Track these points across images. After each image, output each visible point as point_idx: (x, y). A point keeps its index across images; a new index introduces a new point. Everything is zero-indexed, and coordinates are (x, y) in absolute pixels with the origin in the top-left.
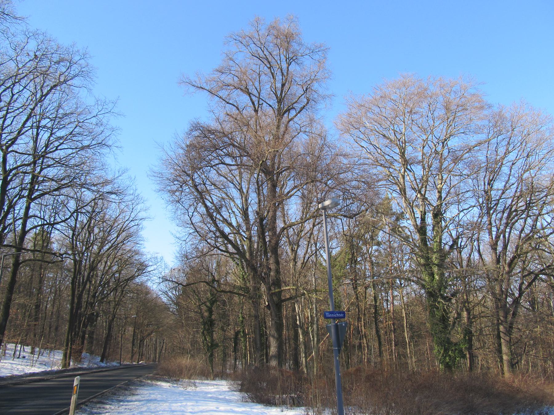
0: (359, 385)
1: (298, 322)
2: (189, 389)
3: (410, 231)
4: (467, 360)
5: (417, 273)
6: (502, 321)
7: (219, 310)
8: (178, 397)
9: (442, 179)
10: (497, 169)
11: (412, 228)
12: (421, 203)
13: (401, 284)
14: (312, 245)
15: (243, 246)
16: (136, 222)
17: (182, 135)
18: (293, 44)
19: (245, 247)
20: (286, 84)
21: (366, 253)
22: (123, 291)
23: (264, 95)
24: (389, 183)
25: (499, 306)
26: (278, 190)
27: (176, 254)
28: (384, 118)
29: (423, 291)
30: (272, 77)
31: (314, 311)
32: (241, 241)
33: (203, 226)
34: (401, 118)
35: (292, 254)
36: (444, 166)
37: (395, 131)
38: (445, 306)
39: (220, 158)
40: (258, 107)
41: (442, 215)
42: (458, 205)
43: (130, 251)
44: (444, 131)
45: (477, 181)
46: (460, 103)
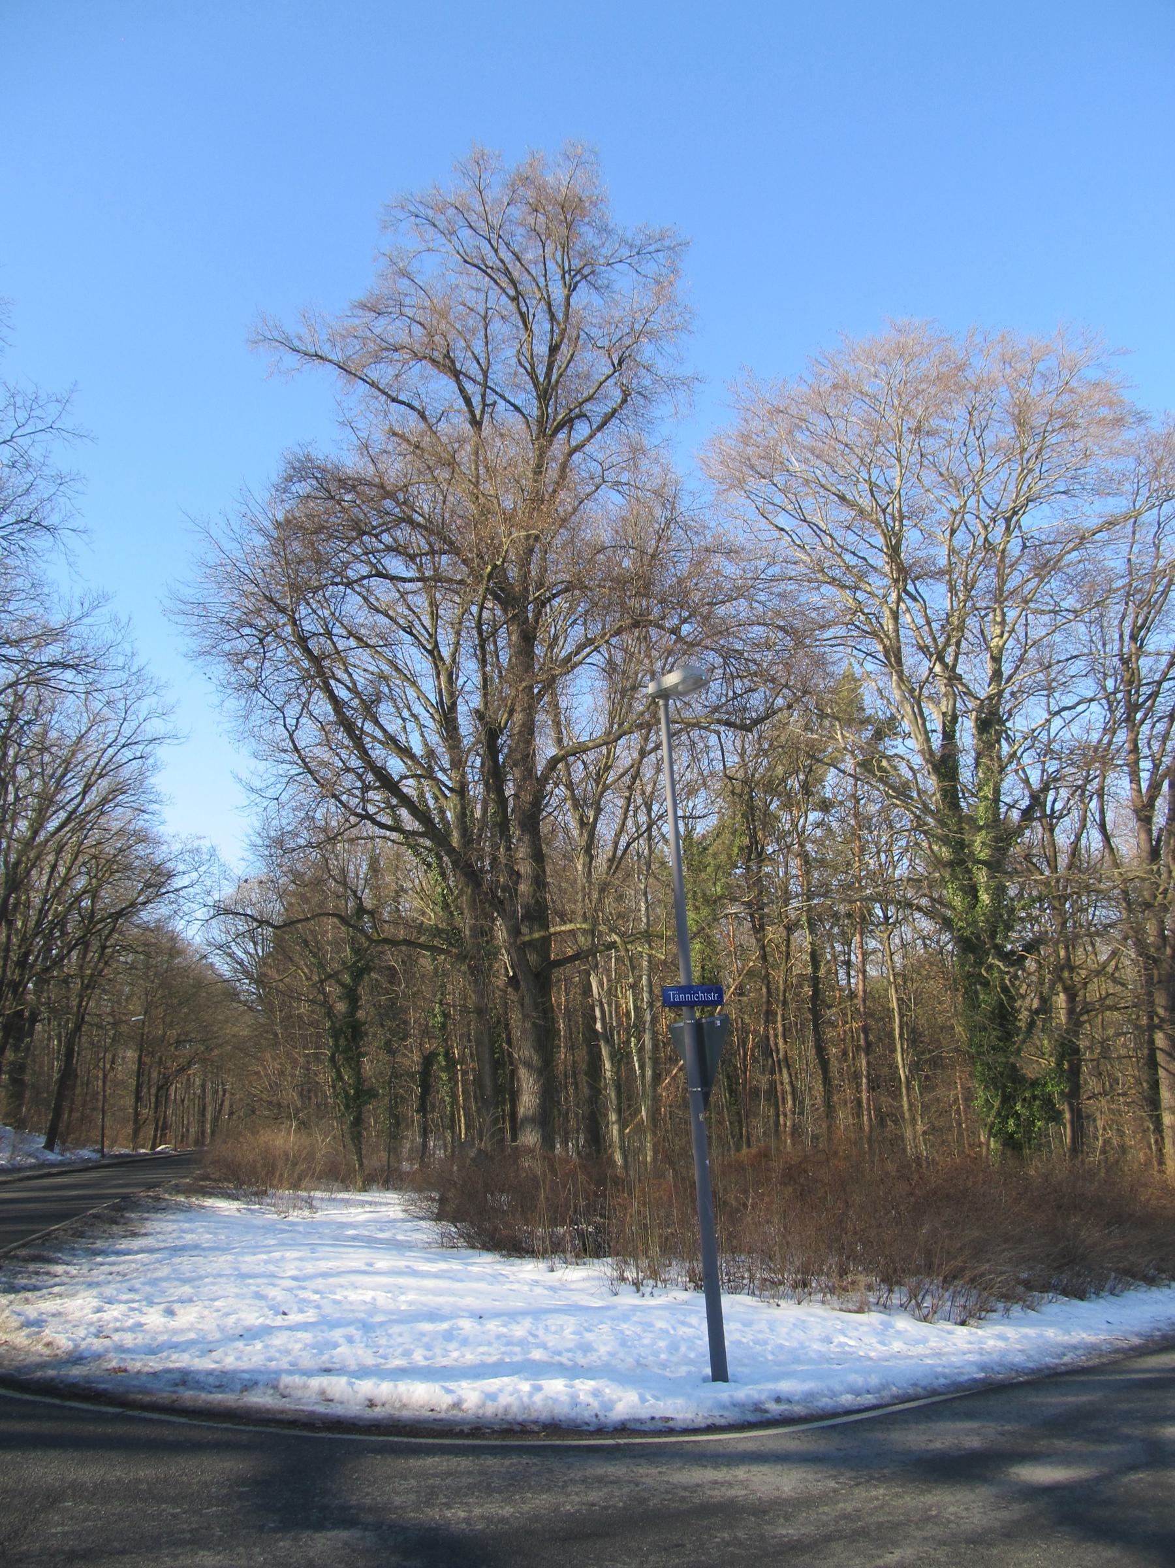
0: (763, 1194)
1: (599, 1026)
2: (295, 1216)
3: (911, 769)
4: (1065, 1128)
5: (930, 887)
6: (1162, 1020)
7: (379, 994)
8: (261, 1238)
9: (1003, 623)
10: (1156, 596)
11: (917, 760)
12: (943, 689)
13: (887, 918)
14: (637, 808)
15: (442, 811)
16: (138, 750)
17: (263, 495)
18: (585, 229)
19: (449, 815)
20: (563, 347)
21: (789, 833)
22: (104, 947)
23: (499, 375)
24: (855, 634)
25: (1156, 979)
26: (539, 650)
27: (253, 838)
28: (842, 447)
29: (945, 937)
30: (521, 325)
31: (645, 995)
32: (436, 799)
33: (324, 754)
34: (891, 447)
35: (581, 834)
36: (1010, 585)
37: (873, 487)
38: (1007, 977)
39: (372, 559)
40: (483, 412)
41: (1003, 723)
42: (1048, 696)
43: (121, 832)
44: (1012, 487)
45: (1102, 627)
46: (1057, 407)
